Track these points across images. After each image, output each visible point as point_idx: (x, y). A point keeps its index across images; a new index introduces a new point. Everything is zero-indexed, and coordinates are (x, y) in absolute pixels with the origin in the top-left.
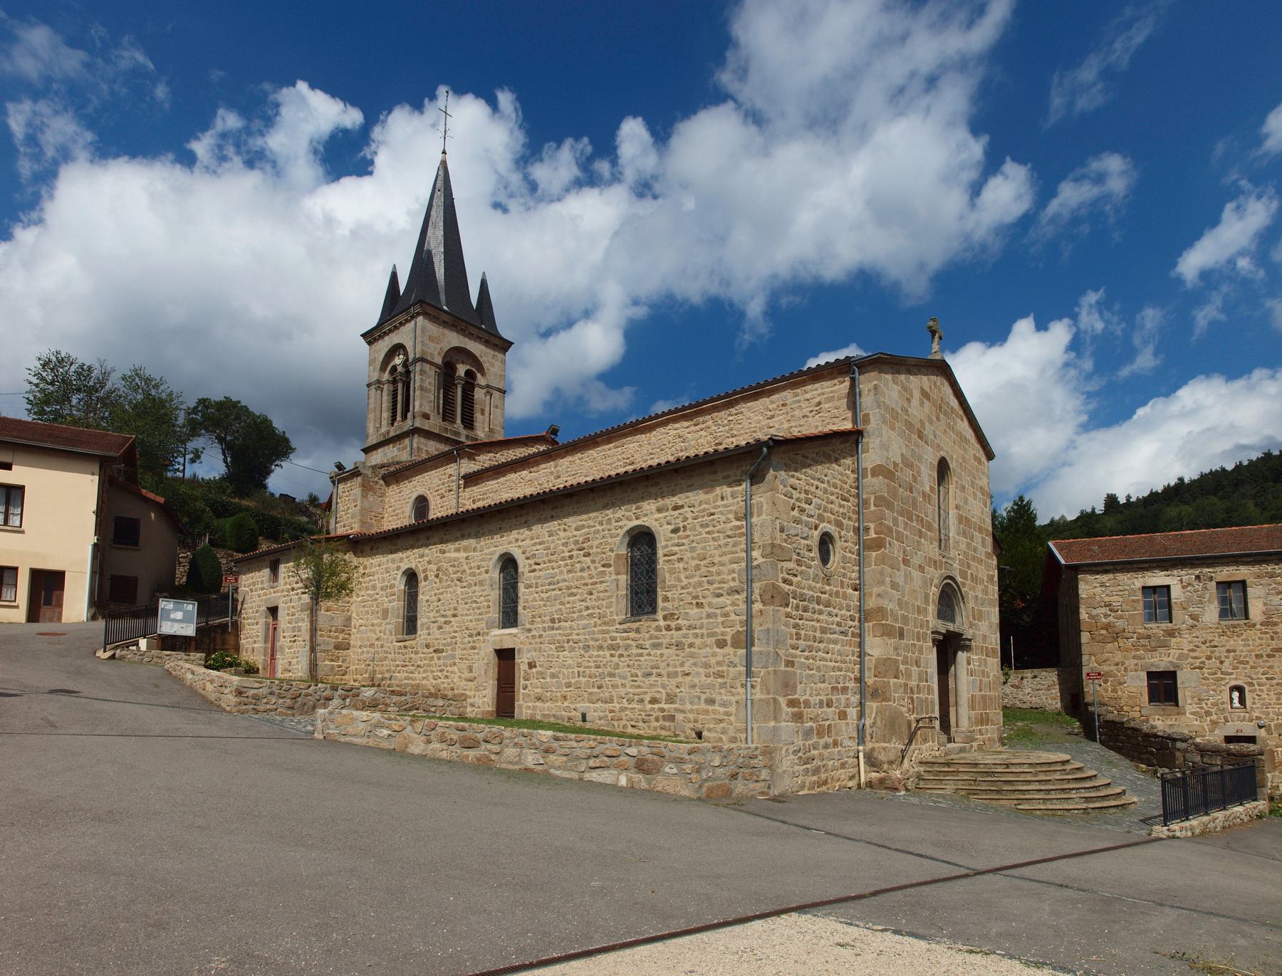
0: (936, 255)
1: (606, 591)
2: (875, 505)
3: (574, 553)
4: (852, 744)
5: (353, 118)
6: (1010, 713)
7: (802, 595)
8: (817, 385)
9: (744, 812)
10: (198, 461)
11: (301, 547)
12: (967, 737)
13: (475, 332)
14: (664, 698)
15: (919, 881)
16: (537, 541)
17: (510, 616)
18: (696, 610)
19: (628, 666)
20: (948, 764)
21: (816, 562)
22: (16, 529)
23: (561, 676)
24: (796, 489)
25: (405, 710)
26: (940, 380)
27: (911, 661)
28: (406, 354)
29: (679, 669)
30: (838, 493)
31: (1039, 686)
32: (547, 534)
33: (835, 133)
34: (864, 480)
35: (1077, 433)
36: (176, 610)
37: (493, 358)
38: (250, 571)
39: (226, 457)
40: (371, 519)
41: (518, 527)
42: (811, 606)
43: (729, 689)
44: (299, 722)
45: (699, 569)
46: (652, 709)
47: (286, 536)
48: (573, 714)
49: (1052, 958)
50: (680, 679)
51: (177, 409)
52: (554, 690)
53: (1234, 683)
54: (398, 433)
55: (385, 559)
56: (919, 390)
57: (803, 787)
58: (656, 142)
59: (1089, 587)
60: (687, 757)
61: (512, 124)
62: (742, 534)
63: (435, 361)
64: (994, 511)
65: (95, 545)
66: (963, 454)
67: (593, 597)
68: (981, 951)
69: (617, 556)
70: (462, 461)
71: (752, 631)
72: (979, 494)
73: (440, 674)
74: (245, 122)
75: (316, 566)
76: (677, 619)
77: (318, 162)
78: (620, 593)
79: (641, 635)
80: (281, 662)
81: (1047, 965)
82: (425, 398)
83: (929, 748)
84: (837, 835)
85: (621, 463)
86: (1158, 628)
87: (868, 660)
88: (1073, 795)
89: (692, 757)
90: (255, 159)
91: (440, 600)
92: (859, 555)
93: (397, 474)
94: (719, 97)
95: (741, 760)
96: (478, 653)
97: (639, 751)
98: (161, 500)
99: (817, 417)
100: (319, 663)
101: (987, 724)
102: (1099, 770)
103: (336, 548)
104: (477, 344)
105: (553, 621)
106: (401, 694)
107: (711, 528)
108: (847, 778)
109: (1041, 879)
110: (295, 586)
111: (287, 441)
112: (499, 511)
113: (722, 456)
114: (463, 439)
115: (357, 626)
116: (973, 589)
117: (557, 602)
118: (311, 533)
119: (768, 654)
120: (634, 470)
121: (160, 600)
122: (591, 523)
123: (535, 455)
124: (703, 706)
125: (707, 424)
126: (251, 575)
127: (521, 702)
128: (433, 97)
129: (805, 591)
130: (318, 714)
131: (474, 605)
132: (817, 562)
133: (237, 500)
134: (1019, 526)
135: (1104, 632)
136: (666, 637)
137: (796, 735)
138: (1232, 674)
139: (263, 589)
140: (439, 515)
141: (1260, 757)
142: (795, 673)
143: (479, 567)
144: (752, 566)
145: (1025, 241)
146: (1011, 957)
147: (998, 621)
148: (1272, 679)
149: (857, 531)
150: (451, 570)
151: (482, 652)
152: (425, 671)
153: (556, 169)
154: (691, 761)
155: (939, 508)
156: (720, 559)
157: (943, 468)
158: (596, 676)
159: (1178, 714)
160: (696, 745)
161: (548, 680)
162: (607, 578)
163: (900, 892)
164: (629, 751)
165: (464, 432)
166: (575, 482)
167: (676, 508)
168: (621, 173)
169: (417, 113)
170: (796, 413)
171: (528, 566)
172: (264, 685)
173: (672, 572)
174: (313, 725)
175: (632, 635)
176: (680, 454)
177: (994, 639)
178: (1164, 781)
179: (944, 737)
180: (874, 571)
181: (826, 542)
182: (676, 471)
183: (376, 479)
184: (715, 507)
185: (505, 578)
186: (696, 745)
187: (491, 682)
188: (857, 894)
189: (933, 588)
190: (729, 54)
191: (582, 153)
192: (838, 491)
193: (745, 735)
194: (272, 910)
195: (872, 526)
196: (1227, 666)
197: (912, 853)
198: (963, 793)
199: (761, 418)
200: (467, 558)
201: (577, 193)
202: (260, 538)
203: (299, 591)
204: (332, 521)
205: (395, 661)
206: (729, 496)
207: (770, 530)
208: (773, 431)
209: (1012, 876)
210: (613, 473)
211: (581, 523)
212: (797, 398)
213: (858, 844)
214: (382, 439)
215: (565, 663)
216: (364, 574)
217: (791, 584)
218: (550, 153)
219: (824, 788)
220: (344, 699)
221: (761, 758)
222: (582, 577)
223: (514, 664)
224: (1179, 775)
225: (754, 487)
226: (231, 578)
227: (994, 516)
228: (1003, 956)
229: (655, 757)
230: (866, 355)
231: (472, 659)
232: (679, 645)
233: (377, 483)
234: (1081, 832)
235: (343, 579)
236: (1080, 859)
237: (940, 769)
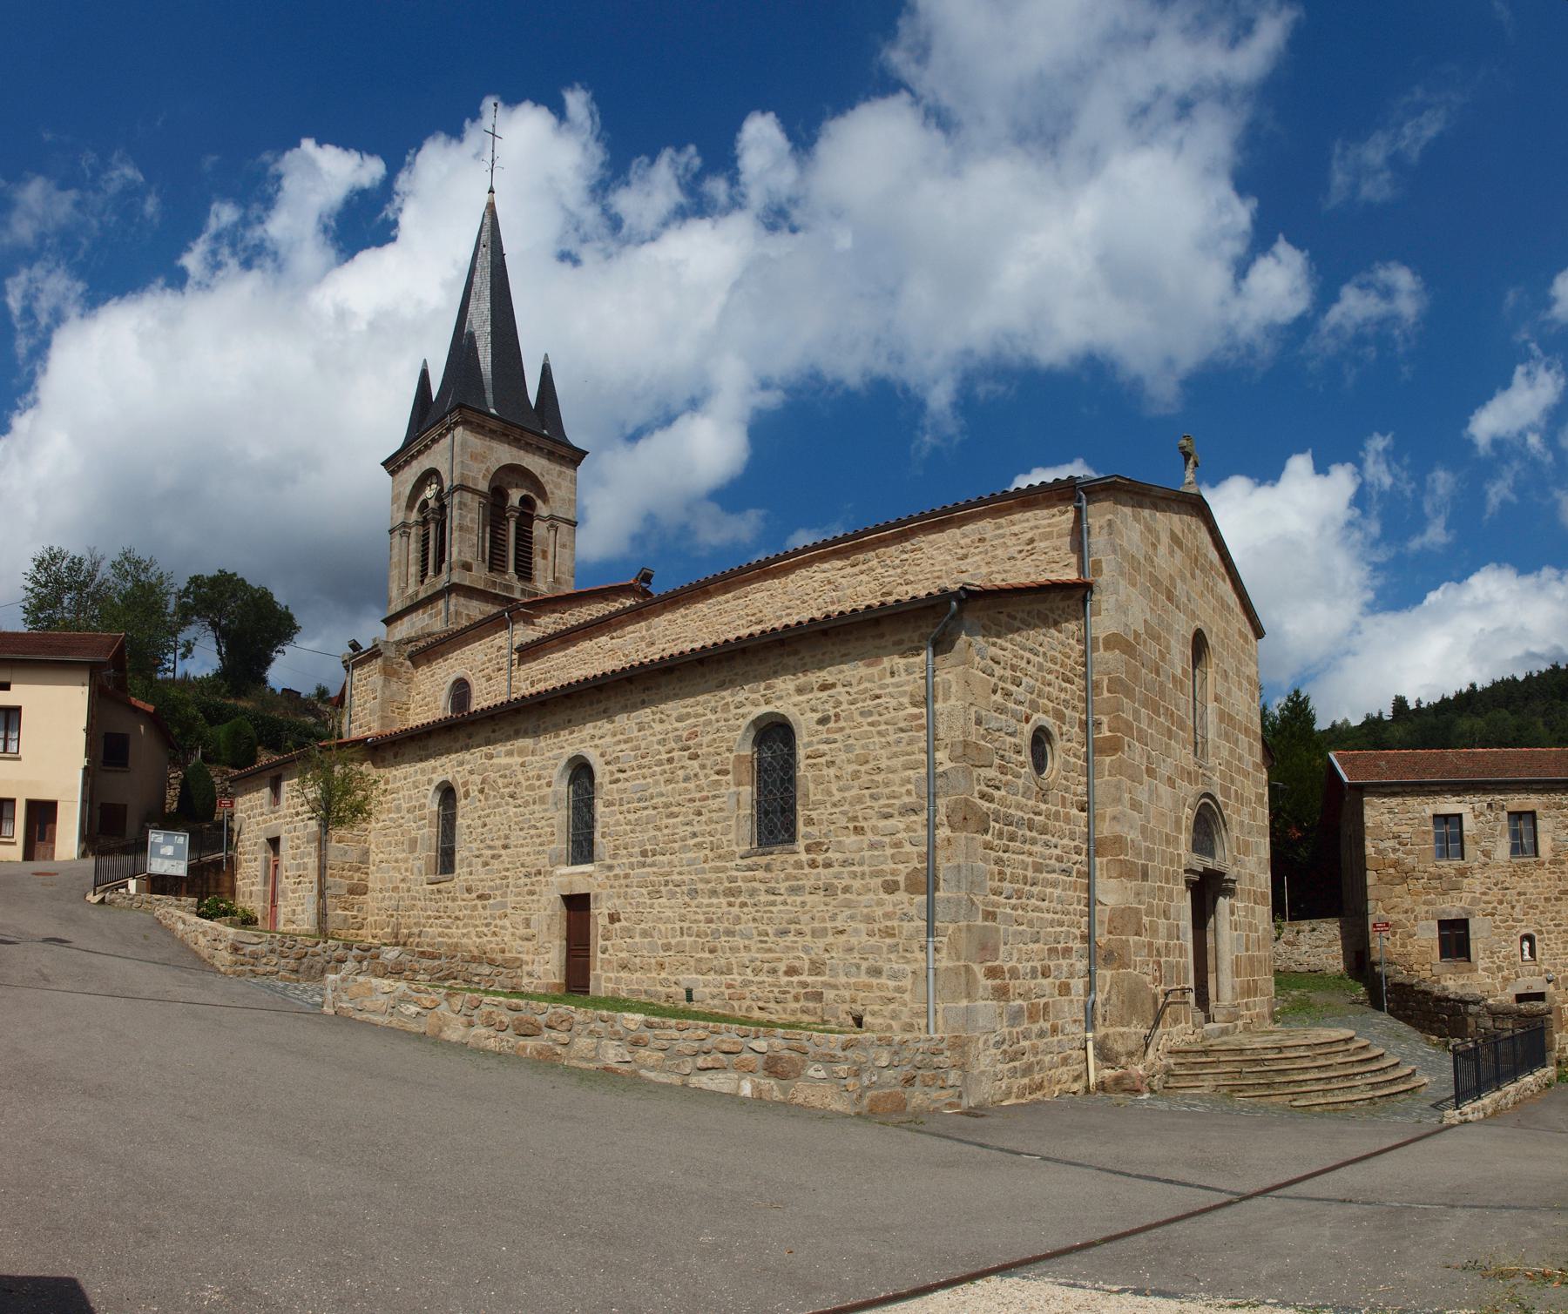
0: (1189, 356)
1: (721, 810)
2: (1109, 691)
3: (675, 754)
4: (1078, 1030)
5: (371, 170)
6: (1285, 979)
7: (1007, 816)
8: (1029, 514)
9: (924, 1132)
10: (190, 656)
11: (306, 758)
12: (1230, 1014)
13: (533, 440)
14: (806, 967)
15: (1168, 1217)
16: (622, 737)
17: (582, 847)
18: (854, 838)
19: (754, 920)
20: (1205, 1053)
21: (1027, 769)
22: (13, 756)
23: (656, 934)
24: (998, 663)
25: (439, 979)
26: (1195, 523)
27: (1158, 911)
28: (440, 482)
29: (829, 925)
30: (1057, 671)
31: (1319, 943)
32: (635, 728)
33: (1054, 153)
34: (1095, 655)
35: (1362, 614)
36: (166, 843)
37: (559, 476)
38: (247, 791)
39: (220, 647)
40: (393, 712)
41: (595, 717)
42: (1020, 833)
43: (902, 953)
44: (305, 991)
45: (859, 778)
46: (790, 984)
47: (289, 743)
48: (674, 989)
49: (1334, 1297)
50: (830, 939)
51: (167, 593)
52: (646, 954)
53: (1525, 931)
54: (429, 593)
55: (412, 769)
56: (1168, 534)
57: (1008, 1094)
58: (795, 149)
59: (1375, 812)
60: (840, 1054)
61: (586, 136)
62: (921, 727)
63: (479, 488)
64: (1264, 708)
65: (86, 769)
66: (1225, 628)
67: (703, 818)
68: (1248, 1304)
69: (738, 757)
70: (516, 627)
71: (935, 869)
72: (1245, 682)
73: (485, 930)
74: (242, 211)
75: (326, 782)
76: (827, 851)
77: (329, 242)
78: (742, 812)
79: (773, 875)
80: (283, 911)
81: (1327, 1307)
82: (465, 542)
83: (1181, 1032)
84: (1057, 1161)
85: (744, 622)
86: (1449, 866)
87: (1100, 910)
88: (1358, 1081)
89: (848, 1053)
90: (254, 255)
91: (485, 825)
92: (1087, 760)
93: (427, 651)
94: (887, 85)
95: (919, 1057)
96: (538, 901)
97: (770, 1045)
98: (150, 708)
99: (1028, 560)
100: (329, 912)
101: (1255, 995)
102: (1387, 1047)
103: (350, 756)
104: (536, 458)
105: (644, 854)
106: (433, 957)
107: (875, 718)
108: (1071, 1080)
109: (1321, 1197)
110: (300, 809)
111: (290, 618)
112: (568, 696)
113: (893, 611)
114: (517, 595)
115: (377, 863)
116: (1238, 812)
117: (650, 826)
118: (319, 738)
119: (959, 902)
120: (763, 632)
121: (150, 831)
122: (700, 710)
123: (618, 613)
124: (864, 978)
125: (870, 564)
126: (248, 797)
127: (599, 972)
128: (476, 115)
129: (1012, 811)
130: (329, 980)
131: (533, 832)
132: (1028, 770)
133: (232, 701)
134: (1295, 729)
135: (1392, 871)
136: (811, 877)
137: (998, 1019)
138: (1522, 920)
139: (262, 814)
140: (485, 705)
141: (1548, 1016)
142: (997, 930)
143: (539, 778)
144: (935, 774)
145: (1302, 352)
146: (1285, 1305)
147: (1268, 856)
148: (1560, 925)
149: (1084, 725)
150: (500, 782)
151: (543, 899)
152: (465, 926)
153: (649, 194)
154: (847, 1059)
155: (1195, 699)
156: (889, 763)
157: (1199, 644)
158: (707, 935)
159: (1470, 971)
160: (854, 1036)
161: (637, 939)
162: (723, 791)
163: (1142, 1235)
164: (755, 1044)
165: (518, 585)
166: (676, 651)
167: (824, 687)
168: (743, 196)
169: (454, 142)
170: (999, 552)
171: (608, 774)
172: (264, 939)
173: (818, 781)
174: (321, 995)
175: (760, 874)
176: (831, 608)
177: (1264, 880)
178: (1456, 1053)
179: (1201, 1015)
180: (1107, 783)
181: (1041, 739)
182: (825, 633)
183: (401, 660)
184: (881, 687)
185: (575, 792)
186: (854, 1036)
187: (557, 942)
188: (1084, 1241)
189: (1187, 809)
190: (903, 23)
191: (687, 168)
192: (1057, 667)
193: (925, 1021)
194: (272, 1235)
195: (1105, 719)
196: (1517, 913)
197: (1158, 1180)
198: (1225, 1090)
199: (949, 558)
200: (523, 765)
201: (680, 228)
202: (259, 748)
203: (305, 816)
204: (346, 720)
205: (426, 910)
206: (902, 671)
207: (962, 721)
208: (966, 578)
209: (1286, 1197)
210: (732, 636)
211: (685, 711)
212: (1000, 531)
213: (1086, 1170)
214: (408, 603)
215: (662, 915)
216: (386, 790)
217: (992, 800)
218: (640, 172)
219: (1038, 1095)
220: (360, 962)
221: (948, 1053)
222: (687, 790)
223: (589, 916)
224: (1471, 1045)
225: (939, 658)
226: (226, 801)
227: (1264, 715)
228: (1275, 1305)
229: (794, 1055)
230: (1096, 477)
231: (530, 909)
232: (828, 889)
233: (402, 665)
234: (1367, 1129)
235: (359, 798)
236: (1365, 1164)
237: (1194, 1059)
